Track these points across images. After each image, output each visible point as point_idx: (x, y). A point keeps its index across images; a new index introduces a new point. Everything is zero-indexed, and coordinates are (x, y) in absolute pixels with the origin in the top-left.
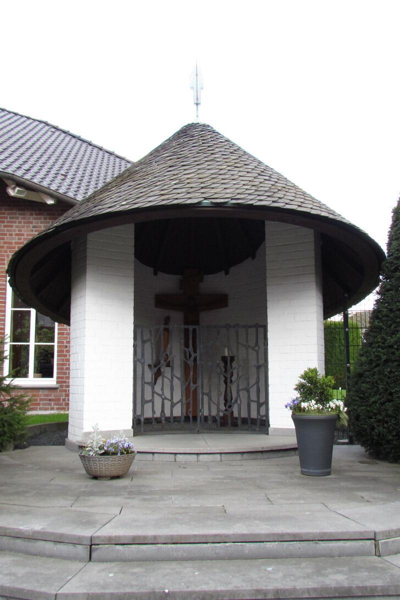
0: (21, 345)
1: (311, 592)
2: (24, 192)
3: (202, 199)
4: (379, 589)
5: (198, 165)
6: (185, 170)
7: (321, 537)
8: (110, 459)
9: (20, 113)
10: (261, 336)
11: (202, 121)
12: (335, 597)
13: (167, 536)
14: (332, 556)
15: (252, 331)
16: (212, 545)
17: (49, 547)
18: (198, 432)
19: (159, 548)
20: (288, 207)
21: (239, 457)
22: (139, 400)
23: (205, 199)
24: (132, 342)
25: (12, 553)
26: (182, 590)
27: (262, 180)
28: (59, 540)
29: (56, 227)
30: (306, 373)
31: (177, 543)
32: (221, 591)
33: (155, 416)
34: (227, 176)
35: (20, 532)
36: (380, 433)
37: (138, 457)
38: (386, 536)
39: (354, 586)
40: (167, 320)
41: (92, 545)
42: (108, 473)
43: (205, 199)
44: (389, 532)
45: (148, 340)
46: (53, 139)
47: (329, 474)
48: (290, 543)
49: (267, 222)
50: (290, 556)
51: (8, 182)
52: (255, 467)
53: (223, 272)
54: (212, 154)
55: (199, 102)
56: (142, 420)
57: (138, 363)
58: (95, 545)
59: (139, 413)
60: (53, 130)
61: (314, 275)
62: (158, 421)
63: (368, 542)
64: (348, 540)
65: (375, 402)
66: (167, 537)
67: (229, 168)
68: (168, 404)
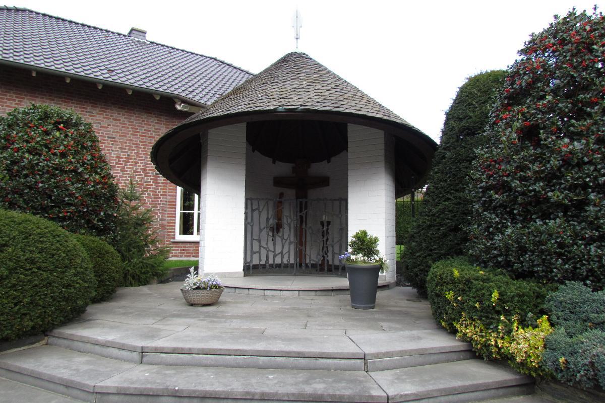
0: (189, 213)
1: (290, 396)
2: (188, 107)
3: (277, 106)
4: (345, 397)
5: (284, 82)
6: (273, 86)
7: (320, 355)
8: (201, 292)
9: (205, 55)
10: (343, 208)
11: (299, 51)
12: (310, 401)
13: (199, 349)
14: (329, 370)
15: (337, 203)
16: (234, 357)
17: (115, 352)
18: (295, 275)
19: (194, 357)
20: (347, 111)
21: (313, 293)
22: (249, 249)
23: (280, 106)
24: (243, 211)
25: (93, 355)
26: (189, 389)
27: (338, 96)
28: (122, 347)
29: (174, 129)
30: (357, 234)
31: (208, 354)
32: (219, 391)
33: (262, 263)
34: (304, 89)
35: (97, 341)
36: (422, 279)
37: (226, 290)
38: (375, 357)
39: (325, 393)
40: (281, 195)
41: (143, 352)
42: (199, 302)
43: (280, 106)
44: (378, 354)
45: (256, 209)
46: (218, 69)
47: (373, 307)
48: (296, 358)
49: (348, 124)
50: (296, 368)
51: (176, 100)
52: (322, 300)
53: (326, 161)
54: (299, 74)
55: (298, 37)
56: (251, 265)
57: (248, 225)
58: (145, 352)
59: (248, 260)
60: (220, 63)
61: (384, 162)
62: (264, 266)
63: (359, 361)
64: (343, 358)
65: (420, 256)
66: (199, 349)
67: (308, 84)
68: (271, 255)
